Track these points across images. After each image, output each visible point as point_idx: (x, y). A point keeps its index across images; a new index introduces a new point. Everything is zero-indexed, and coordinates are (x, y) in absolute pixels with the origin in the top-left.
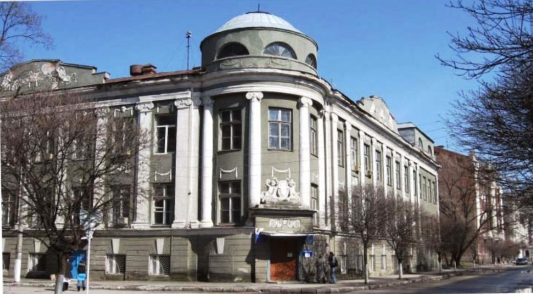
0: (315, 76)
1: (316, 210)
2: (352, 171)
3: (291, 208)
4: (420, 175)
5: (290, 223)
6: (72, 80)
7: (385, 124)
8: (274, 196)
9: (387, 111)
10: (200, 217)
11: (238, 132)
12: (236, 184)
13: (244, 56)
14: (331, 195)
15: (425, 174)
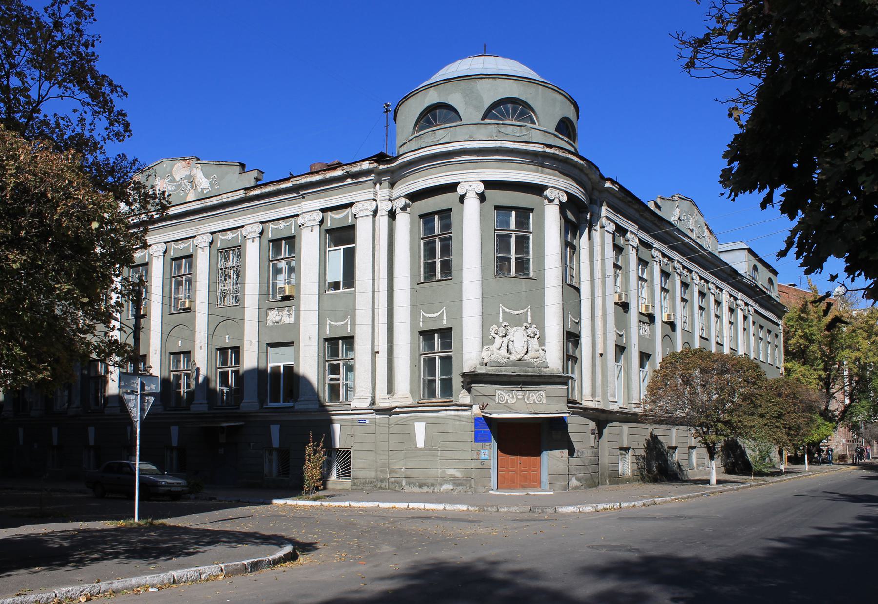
0: (570, 152)
1: (570, 375)
2: (616, 304)
3: (530, 371)
4: (754, 323)
5: (528, 398)
6: (211, 185)
7: (698, 241)
8: (503, 351)
9: (701, 220)
10: (390, 390)
11: (447, 249)
12: (446, 334)
13: (454, 124)
14: (180, 287)
15: (763, 322)
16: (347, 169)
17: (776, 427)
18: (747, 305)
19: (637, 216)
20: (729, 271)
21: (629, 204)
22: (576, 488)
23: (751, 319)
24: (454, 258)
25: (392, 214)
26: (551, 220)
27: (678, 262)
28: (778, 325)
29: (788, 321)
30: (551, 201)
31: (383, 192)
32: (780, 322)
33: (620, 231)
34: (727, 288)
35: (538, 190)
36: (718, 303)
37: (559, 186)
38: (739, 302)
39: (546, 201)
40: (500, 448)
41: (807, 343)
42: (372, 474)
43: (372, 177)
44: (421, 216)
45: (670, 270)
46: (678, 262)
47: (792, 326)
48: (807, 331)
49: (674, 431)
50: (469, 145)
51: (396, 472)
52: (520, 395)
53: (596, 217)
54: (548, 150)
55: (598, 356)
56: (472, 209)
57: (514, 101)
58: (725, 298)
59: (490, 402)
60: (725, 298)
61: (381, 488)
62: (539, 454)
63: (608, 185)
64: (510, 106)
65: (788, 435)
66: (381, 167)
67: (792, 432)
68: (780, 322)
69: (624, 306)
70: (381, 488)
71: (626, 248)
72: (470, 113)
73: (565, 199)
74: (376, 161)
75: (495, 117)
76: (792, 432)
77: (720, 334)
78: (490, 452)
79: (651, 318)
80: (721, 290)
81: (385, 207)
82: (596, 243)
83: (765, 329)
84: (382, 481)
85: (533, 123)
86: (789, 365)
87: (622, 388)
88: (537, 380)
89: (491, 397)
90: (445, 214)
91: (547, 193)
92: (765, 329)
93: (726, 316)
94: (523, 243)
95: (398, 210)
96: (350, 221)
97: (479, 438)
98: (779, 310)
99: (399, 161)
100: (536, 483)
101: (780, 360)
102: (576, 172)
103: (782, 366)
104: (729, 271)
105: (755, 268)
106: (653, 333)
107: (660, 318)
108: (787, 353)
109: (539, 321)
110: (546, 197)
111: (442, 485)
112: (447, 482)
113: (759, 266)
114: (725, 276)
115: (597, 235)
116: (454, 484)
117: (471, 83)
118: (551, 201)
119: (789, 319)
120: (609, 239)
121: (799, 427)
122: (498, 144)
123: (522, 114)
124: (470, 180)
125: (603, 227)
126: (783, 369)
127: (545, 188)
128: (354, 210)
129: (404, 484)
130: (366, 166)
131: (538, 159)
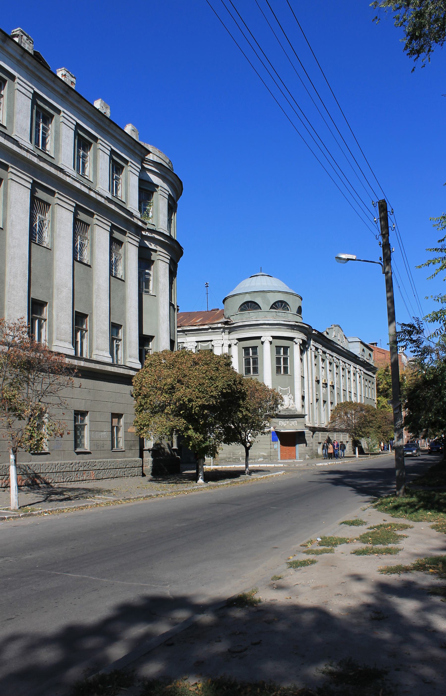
16: (211, 326)
17: (378, 432)
18: (360, 370)
19: (322, 341)
20: (354, 356)
21: (322, 339)
22: (308, 459)
23: (362, 377)
24: (259, 366)
25: (230, 346)
26: (296, 349)
27: (335, 357)
28: (374, 378)
29: (379, 375)
30: (296, 343)
31: (225, 336)
32: (374, 376)
33: (317, 349)
34: (352, 364)
35: (291, 339)
36: (349, 372)
37: (299, 336)
38: (358, 370)
39: (294, 343)
40: (282, 444)
41: (388, 387)
42: (225, 456)
43: (222, 330)
44: (243, 348)
45: (332, 361)
46: (335, 357)
47: (381, 378)
48: (388, 381)
49: (335, 434)
50: (267, 322)
51: (236, 454)
52: (288, 422)
53: (309, 345)
54: (297, 324)
55: (310, 404)
56: (267, 346)
57: (282, 302)
58: (352, 369)
59: (277, 425)
60: (352, 369)
61: (229, 461)
62: (295, 445)
63: (314, 332)
64: (280, 303)
65: (383, 435)
66: (226, 326)
67: (385, 434)
68: (374, 376)
69: (318, 382)
70: (229, 461)
71: (318, 356)
72: (265, 306)
73: (301, 342)
74: (224, 324)
75: (274, 308)
76: (385, 434)
77: (350, 386)
78: (277, 445)
79: (326, 384)
80: (350, 365)
81: (227, 343)
82: (310, 354)
83: (368, 381)
84: (229, 458)
85: (288, 310)
86: (379, 399)
87: (323, 418)
88: (294, 416)
89: (277, 423)
90: (255, 348)
91: (295, 340)
92: (368, 381)
93: (352, 378)
94: (285, 360)
95: (233, 345)
96: (210, 347)
97: (274, 440)
98: (372, 369)
99: (235, 325)
100: (295, 457)
101: (374, 396)
102: (305, 330)
103: (376, 399)
104: (354, 356)
105: (363, 350)
106: (327, 391)
107: (329, 384)
108: (378, 390)
109: (293, 393)
110: (295, 342)
111: (258, 459)
112: (261, 458)
113: (365, 348)
114: (352, 358)
115: (309, 352)
116: (263, 458)
117: (265, 294)
118: (296, 343)
119: (379, 375)
120: (313, 353)
121: (387, 432)
122: (278, 322)
123: (285, 306)
124: (267, 336)
125: (311, 349)
126: (376, 401)
127: (295, 338)
128: (213, 343)
129: (241, 459)
130: (220, 325)
131: (292, 327)
